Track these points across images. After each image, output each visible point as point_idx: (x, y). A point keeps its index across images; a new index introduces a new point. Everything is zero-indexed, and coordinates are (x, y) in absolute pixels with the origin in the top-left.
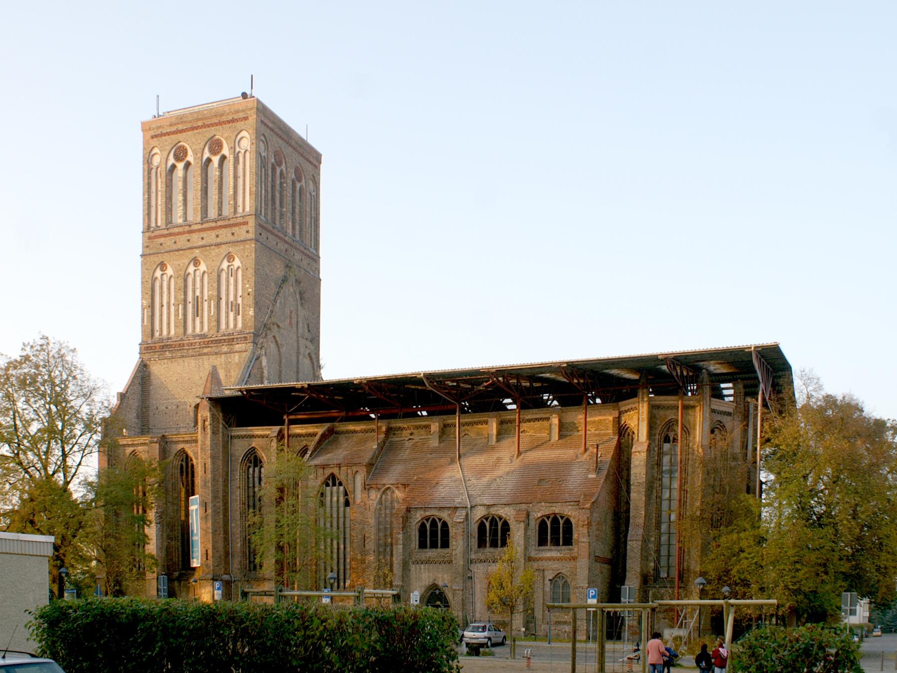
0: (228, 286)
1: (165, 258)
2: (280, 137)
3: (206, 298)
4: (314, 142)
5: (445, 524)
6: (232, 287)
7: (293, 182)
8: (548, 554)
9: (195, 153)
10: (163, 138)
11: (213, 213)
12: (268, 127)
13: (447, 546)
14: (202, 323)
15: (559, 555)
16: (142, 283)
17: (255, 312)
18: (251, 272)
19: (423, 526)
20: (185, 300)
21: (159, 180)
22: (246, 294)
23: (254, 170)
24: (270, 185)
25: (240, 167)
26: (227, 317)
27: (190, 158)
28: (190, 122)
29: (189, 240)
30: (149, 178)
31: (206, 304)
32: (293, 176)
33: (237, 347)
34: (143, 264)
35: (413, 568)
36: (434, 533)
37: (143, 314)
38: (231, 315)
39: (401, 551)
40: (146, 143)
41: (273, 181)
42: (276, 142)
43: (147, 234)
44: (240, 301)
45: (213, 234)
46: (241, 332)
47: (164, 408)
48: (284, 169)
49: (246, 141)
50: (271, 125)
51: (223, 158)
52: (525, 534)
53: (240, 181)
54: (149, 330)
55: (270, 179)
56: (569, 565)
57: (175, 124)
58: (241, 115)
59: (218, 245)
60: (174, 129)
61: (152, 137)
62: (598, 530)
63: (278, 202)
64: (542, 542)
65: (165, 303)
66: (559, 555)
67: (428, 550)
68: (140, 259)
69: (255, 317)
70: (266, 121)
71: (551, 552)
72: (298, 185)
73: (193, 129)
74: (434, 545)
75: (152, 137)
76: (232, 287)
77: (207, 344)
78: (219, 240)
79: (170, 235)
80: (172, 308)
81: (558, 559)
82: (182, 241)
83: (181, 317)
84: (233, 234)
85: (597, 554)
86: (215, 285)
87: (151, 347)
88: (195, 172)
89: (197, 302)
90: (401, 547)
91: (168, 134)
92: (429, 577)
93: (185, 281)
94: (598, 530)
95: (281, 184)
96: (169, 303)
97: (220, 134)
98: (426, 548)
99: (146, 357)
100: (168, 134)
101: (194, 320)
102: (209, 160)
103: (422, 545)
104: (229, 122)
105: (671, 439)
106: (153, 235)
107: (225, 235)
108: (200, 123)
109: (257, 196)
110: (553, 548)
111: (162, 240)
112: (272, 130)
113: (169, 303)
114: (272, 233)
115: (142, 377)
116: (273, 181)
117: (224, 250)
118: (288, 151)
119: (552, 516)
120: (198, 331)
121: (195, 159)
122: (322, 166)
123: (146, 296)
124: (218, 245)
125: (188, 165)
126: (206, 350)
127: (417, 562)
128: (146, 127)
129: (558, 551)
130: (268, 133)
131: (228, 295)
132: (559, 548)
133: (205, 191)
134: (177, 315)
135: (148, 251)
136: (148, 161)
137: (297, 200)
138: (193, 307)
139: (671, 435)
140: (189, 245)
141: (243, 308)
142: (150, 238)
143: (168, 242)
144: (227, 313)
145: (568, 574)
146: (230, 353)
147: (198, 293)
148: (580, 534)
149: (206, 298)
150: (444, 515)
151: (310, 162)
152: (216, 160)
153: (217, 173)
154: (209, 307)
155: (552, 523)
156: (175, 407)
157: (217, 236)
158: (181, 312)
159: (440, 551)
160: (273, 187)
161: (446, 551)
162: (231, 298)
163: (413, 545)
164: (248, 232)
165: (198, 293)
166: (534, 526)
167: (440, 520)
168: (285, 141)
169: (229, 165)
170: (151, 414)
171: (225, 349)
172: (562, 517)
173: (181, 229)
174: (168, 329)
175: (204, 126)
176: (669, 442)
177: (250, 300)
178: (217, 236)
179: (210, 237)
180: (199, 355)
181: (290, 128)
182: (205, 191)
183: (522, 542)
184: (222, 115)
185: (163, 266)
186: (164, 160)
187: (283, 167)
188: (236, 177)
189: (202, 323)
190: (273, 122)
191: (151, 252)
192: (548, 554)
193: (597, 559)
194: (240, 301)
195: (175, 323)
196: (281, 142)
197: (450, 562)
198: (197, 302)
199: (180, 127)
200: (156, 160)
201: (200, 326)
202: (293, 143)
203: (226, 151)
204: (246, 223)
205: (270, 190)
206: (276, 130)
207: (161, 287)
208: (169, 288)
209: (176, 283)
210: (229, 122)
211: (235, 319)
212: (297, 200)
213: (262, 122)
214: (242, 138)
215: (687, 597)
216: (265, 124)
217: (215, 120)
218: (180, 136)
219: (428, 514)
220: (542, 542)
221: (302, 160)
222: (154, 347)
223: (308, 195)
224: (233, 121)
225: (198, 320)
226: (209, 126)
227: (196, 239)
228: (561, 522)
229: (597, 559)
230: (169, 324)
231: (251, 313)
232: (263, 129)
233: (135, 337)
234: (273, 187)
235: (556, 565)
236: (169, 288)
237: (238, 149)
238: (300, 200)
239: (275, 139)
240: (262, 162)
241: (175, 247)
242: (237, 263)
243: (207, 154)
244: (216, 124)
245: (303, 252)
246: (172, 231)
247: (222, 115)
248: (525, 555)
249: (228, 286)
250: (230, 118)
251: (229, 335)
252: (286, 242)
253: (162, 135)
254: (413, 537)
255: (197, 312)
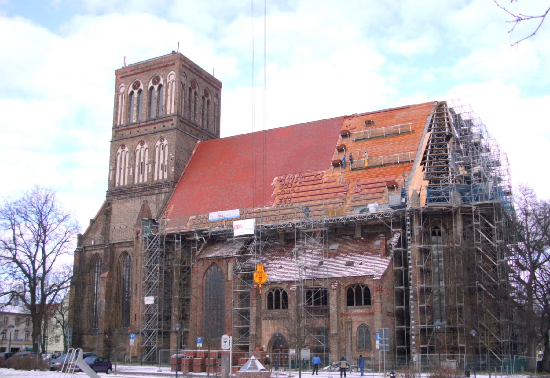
0: (159, 156)
1: (125, 141)
2: (195, 74)
3: (146, 162)
4: (218, 76)
5: (285, 293)
6: (162, 156)
7: (203, 98)
8: (355, 311)
9: (144, 84)
10: (127, 78)
11: (153, 116)
12: (187, 68)
13: (369, 304)
14: (143, 177)
15: (361, 311)
16: (111, 156)
17: (175, 170)
18: (173, 147)
19: (270, 295)
20: (134, 165)
21: (123, 100)
22: (170, 159)
23: (177, 91)
24: (187, 99)
25: (169, 90)
26: (158, 173)
27: (141, 87)
28: (142, 68)
29: (138, 131)
30: (118, 99)
31: (146, 167)
32: (203, 94)
33: (164, 190)
34: (112, 146)
35: (263, 322)
36: (277, 299)
37: (110, 174)
38: (161, 172)
39: (255, 311)
40: (117, 81)
41: (190, 96)
42: (192, 76)
43: (115, 130)
44: (166, 163)
45: (152, 127)
46: (166, 182)
47: (118, 228)
48: (210, 99)
49: (173, 76)
50: (189, 67)
51: (160, 86)
52: (338, 298)
53: (169, 98)
54: (112, 183)
55: (188, 96)
56: (368, 318)
57: (134, 70)
58: (171, 63)
59: (155, 133)
60: (133, 72)
61: (121, 78)
62: (388, 294)
63: (193, 108)
64: (350, 303)
65: (123, 167)
66: (361, 311)
67: (273, 310)
68: (110, 144)
69: (175, 172)
70: (186, 65)
71: (356, 310)
72: (206, 99)
73: (144, 72)
74: (277, 307)
75: (121, 78)
76: (162, 156)
77: (144, 189)
78: (156, 130)
79: (128, 129)
80: (127, 170)
81: (361, 314)
82: (135, 132)
83: (131, 174)
84: (164, 126)
85: (388, 311)
86: (152, 155)
87: (113, 193)
88: (145, 94)
89: (142, 165)
90: (255, 308)
91: (130, 75)
92: (274, 328)
93: (135, 154)
94: (388, 294)
95: (195, 98)
96: (125, 167)
97: (157, 73)
98: (272, 308)
99: (111, 198)
100: (130, 75)
101: (139, 176)
102: (152, 88)
103: (270, 307)
104: (164, 67)
105: (437, 233)
106: (118, 130)
107: (159, 127)
108: (148, 69)
109: (178, 104)
110: (357, 307)
111: (123, 132)
112: (190, 70)
113: (125, 167)
114: (188, 125)
115: (106, 211)
116: (190, 96)
117: (158, 135)
118: (199, 81)
119: (356, 285)
120: (141, 181)
121: (144, 87)
122: (222, 89)
123: (112, 164)
124: (155, 133)
125: (140, 91)
126: (145, 193)
127: (266, 319)
128: (118, 72)
129: (361, 308)
130: (187, 71)
131: (159, 160)
132: (361, 307)
133: (150, 104)
134: (129, 173)
135: (115, 139)
136: (117, 90)
137: (206, 108)
138: (139, 169)
139: (437, 231)
140: (138, 134)
141: (168, 167)
142: (116, 132)
143: (127, 133)
144: (158, 171)
145: (368, 324)
146: (159, 194)
147: (142, 160)
148: (375, 297)
149: (146, 162)
150: (284, 287)
151: (215, 87)
152: (156, 87)
153: (157, 94)
154: (148, 168)
155: (356, 290)
156: (125, 227)
157: (155, 128)
158: (131, 171)
159: (281, 310)
160: (190, 100)
161: (285, 310)
162: (161, 162)
163: (263, 308)
164: (172, 125)
165: (142, 160)
166: (343, 292)
167: (281, 290)
168: (198, 76)
169: (164, 89)
170: (111, 232)
171: (156, 191)
172: (281, 290)
173: (134, 126)
174: (123, 181)
175: (150, 70)
176: (435, 235)
177: (173, 163)
178: (155, 128)
179: (151, 128)
180: (141, 196)
181: (201, 69)
182: (150, 104)
183: (335, 304)
184: (160, 64)
185: (123, 146)
186: (126, 89)
187: (197, 89)
188: (167, 95)
189: (143, 177)
190: (190, 66)
191: (117, 139)
192: (355, 311)
193: (388, 314)
194: (166, 163)
195: (128, 178)
196: (195, 76)
197: (288, 318)
198: (142, 165)
199: (137, 71)
200: (122, 90)
201: (141, 179)
202: (204, 77)
203: (162, 82)
204: (172, 120)
205: (187, 101)
206: (192, 69)
207: (121, 159)
208: (125, 159)
209: (130, 155)
210: (164, 67)
211: (163, 174)
212: (206, 108)
213: (183, 65)
214: (171, 74)
215: (400, 348)
216: (185, 67)
217: (157, 66)
218: (136, 76)
219: (273, 286)
220: (350, 303)
221: (209, 86)
222: (115, 193)
223: (213, 105)
224: (167, 66)
225: (141, 176)
226: (153, 69)
227: (142, 130)
228: (363, 289)
229: (388, 314)
230: (124, 179)
231: (173, 170)
232: (184, 69)
233: (105, 187)
234: (190, 100)
235: (360, 319)
236: (125, 159)
237: (168, 81)
238: (208, 107)
239: (191, 74)
240: (182, 85)
241: (130, 136)
242: (165, 142)
243: (151, 84)
244: (157, 68)
245: (209, 136)
246: (129, 127)
247: (160, 64)
248: (338, 312)
249: (159, 156)
250: (165, 64)
251: (159, 183)
252: (197, 130)
253: (127, 76)
254: (263, 302)
255: (142, 171)
